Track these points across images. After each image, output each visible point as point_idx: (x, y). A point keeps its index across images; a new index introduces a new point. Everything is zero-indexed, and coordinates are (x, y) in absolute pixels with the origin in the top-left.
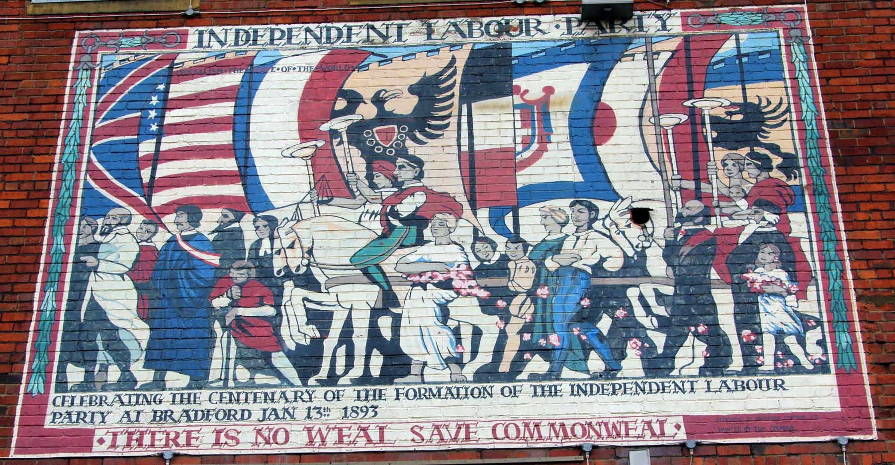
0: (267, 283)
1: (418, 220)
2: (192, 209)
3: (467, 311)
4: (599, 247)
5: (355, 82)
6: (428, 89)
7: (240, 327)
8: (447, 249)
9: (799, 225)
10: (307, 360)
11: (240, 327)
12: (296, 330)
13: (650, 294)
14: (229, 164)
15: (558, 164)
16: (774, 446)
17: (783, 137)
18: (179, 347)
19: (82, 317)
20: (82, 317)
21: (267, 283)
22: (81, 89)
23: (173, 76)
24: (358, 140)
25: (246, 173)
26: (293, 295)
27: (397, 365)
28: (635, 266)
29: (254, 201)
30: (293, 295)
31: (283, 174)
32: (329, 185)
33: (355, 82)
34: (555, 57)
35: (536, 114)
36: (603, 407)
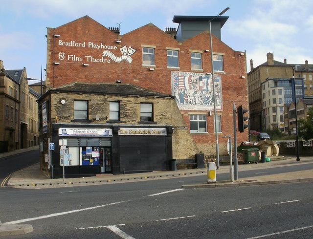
0: (187, 96)
1: (196, 92)
2: (181, 89)
3: (200, 99)
4: (207, 95)
5: (192, 78)
6: (196, 80)
7: (186, 100)
8: (198, 94)
9: (219, 94)
10: (190, 103)
11: (186, 100)
12: (189, 101)
13: (211, 98)
14: (183, 83)
15: (205, 88)
16: (93, 140)
17: (219, 87)
18: (182, 101)
19: (199, 58)
20: (199, 58)
21: (187, 96)
22: (172, 77)
23: (179, 76)
24: (193, 84)
25: (185, 87)
26: (189, 97)
27: (196, 104)
28: (210, 97)
29: (185, 89)
30: (189, 97)
31: (188, 87)
32: (191, 88)
33: (192, 78)
34: (205, 78)
35: (204, 83)
36: (207, 107)
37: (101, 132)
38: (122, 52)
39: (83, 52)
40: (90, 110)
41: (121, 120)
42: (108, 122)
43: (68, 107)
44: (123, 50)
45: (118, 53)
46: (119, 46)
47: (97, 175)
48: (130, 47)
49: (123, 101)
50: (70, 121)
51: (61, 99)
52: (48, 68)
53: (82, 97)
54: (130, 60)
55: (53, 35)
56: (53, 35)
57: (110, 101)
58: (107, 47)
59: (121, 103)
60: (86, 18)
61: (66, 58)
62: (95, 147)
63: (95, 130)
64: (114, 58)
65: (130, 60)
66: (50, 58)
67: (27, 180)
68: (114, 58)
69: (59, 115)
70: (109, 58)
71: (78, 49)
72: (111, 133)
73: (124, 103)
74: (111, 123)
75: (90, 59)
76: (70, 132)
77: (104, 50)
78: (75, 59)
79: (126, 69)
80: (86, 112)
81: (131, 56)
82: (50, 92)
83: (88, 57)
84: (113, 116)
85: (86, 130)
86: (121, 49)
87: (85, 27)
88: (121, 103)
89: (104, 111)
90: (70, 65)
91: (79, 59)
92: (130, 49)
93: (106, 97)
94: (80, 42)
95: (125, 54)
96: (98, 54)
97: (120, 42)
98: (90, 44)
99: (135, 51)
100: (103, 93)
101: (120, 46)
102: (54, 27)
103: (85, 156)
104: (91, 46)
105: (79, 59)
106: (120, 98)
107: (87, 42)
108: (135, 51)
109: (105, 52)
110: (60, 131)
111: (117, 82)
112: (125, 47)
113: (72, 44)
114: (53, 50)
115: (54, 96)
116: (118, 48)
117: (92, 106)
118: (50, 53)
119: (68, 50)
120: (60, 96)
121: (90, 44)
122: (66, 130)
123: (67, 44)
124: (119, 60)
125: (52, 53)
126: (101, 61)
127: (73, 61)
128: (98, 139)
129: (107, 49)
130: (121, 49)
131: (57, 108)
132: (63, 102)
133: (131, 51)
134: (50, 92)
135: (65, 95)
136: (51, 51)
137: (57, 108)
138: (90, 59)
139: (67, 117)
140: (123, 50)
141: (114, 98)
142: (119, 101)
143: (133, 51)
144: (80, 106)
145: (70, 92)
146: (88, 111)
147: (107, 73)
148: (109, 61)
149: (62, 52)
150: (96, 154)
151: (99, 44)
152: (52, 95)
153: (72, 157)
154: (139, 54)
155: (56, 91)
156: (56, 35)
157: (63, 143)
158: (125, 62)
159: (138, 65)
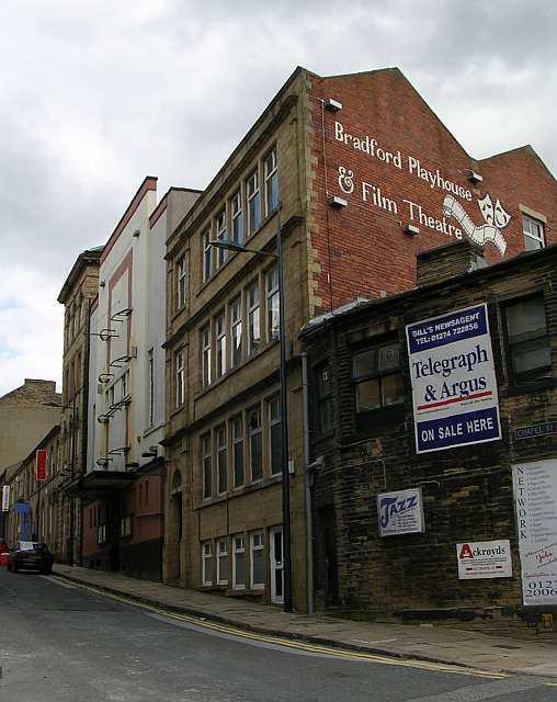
38: (485, 214)
48: (498, 205)
78: (381, 201)
95: (490, 221)
96: (433, 205)
98: (414, 163)
112: (487, 200)
119: (366, 168)
125: (321, 162)
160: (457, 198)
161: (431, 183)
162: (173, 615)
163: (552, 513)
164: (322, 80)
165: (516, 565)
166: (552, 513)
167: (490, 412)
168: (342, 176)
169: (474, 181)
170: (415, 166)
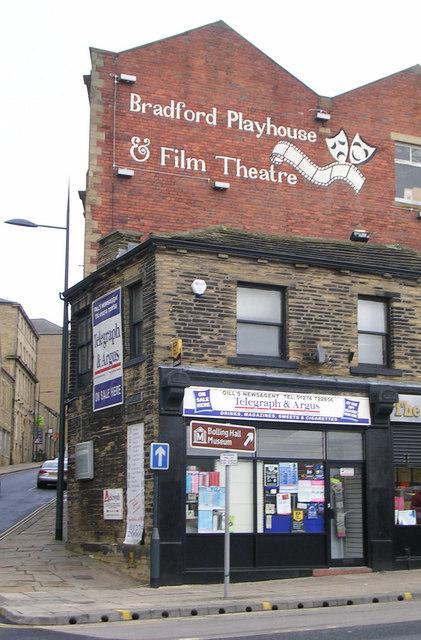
37: (331, 408)
38: (334, 153)
39: (210, 142)
40: (293, 323)
41: (398, 365)
42: (354, 373)
43: (216, 307)
44: (337, 144)
45: (320, 156)
46: (322, 130)
47: (315, 571)
48: (357, 139)
49: (403, 298)
50: (222, 361)
51: (190, 276)
52: (96, 186)
53: (266, 273)
54: (357, 181)
55: (113, 79)
56: (113, 79)
57: (362, 297)
58: (287, 132)
59: (396, 304)
60: (218, 39)
61: (156, 156)
62: (310, 461)
63: (312, 399)
64: (308, 168)
65: (357, 181)
66: (99, 151)
67: (93, 594)
68: (308, 168)
69: (187, 333)
70: (292, 170)
71: (194, 131)
72: (363, 411)
73: (406, 306)
74: (365, 375)
75: (232, 165)
76: (225, 401)
77: (278, 139)
78: (183, 162)
79: (345, 210)
80: (274, 333)
81: (362, 167)
82: (148, 250)
83: (226, 159)
84: (369, 351)
85: (281, 397)
86: (330, 142)
87: (214, 58)
88: (396, 304)
89: (344, 329)
90: (169, 181)
91: (199, 165)
92: (357, 144)
93: (347, 280)
94: (200, 108)
95: (342, 159)
96: (259, 152)
97: (327, 117)
98: (234, 117)
99: (371, 150)
100: (338, 269)
101: (328, 131)
102: (117, 49)
103: (319, 479)
104: (235, 124)
105: (199, 165)
106: (393, 287)
107: (223, 109)
108: (371, 150)
109: (280, 148)
110: (189, 401)
111: (355, 238)
112: (342, 137)
113: (173, 110)
114: (111, 126)
115: (165, 263)
116: (321, 137)
117: (300, 309)
118: (102, 136)
119: (162, 133)
120: (190, 263)
121: (234, 117)
122: (208, 392)
123: (160, 111)
124: (322, 177)
125: (109, 137)
126: (268, 175)
127: (178, 170)
128: (318, 435)
129: (286, 139)
130: (330, 142)
131: (179, 310)
132: (200, 286)
133: (361, 152)
134: (148, 250)
135: (207, 263)
136: (106, 128)
137: (177, 308)
138: (232, 165)
139: (211, 345)
140: (337, 144)
141: (372, 284)
142: (386, 299)
143: (366, 151)
144: (254, 305)
145: (225, 250)
146: (283, 328)
147: (288, 217)
148: (292, 179)
149: (142, 135)
150: (311, 492)
151: (262, 121)
152: (159, 258)
153: (228, 503)
154: (385, 164)
155: (175, 245)
156: (124, 77)
157: (197, 440)
158: (341, 185)
159: (381, 200)
160: (297, 143)
161: (257, 132)
162: (242, 368)
163: (204, 476)
164: (117, 55)
165: (125, 512)
166: (204, 476)
167: (117, 381)
168: (136, 146)
169: (323, 121)
170: (235, 120)
